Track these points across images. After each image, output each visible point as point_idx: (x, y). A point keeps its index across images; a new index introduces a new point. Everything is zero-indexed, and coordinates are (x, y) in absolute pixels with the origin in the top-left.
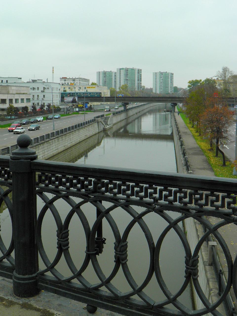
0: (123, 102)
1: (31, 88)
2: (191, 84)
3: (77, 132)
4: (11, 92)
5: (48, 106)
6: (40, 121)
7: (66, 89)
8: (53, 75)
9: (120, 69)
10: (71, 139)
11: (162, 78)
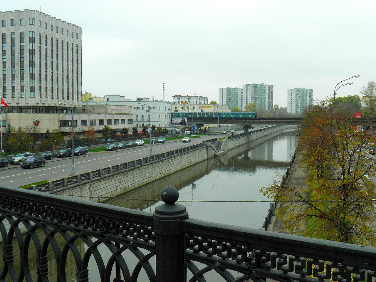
0: (196, 123)
1: (135, 108)
2: (333, 102)
3: (178, 158)
4: (110, 112)
5: (152, 128)
6: (140, 145)
7: (178, 109)
8: (164, 92)
9: (247, 85)
10: (170, 166)
11: (299, 96)
